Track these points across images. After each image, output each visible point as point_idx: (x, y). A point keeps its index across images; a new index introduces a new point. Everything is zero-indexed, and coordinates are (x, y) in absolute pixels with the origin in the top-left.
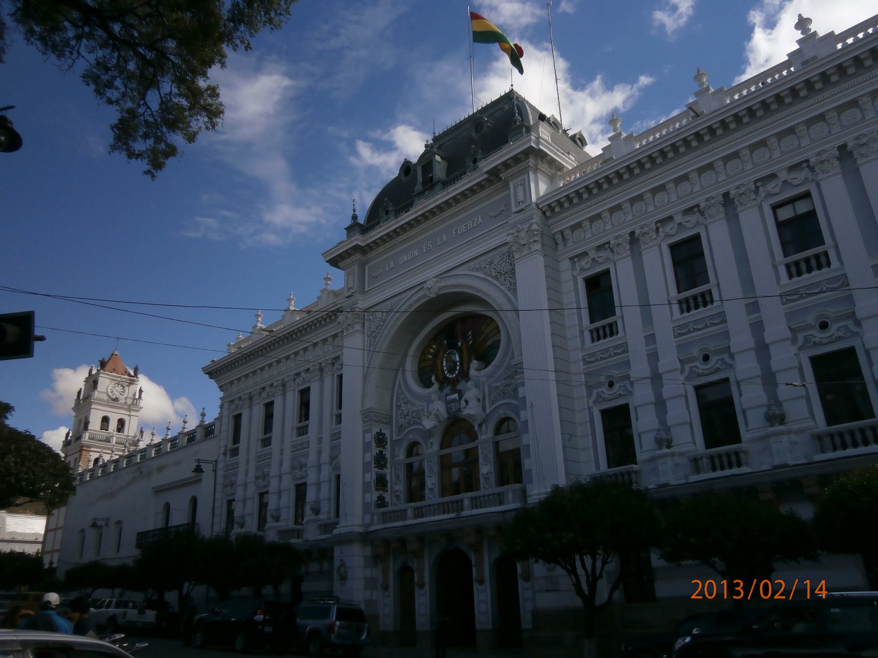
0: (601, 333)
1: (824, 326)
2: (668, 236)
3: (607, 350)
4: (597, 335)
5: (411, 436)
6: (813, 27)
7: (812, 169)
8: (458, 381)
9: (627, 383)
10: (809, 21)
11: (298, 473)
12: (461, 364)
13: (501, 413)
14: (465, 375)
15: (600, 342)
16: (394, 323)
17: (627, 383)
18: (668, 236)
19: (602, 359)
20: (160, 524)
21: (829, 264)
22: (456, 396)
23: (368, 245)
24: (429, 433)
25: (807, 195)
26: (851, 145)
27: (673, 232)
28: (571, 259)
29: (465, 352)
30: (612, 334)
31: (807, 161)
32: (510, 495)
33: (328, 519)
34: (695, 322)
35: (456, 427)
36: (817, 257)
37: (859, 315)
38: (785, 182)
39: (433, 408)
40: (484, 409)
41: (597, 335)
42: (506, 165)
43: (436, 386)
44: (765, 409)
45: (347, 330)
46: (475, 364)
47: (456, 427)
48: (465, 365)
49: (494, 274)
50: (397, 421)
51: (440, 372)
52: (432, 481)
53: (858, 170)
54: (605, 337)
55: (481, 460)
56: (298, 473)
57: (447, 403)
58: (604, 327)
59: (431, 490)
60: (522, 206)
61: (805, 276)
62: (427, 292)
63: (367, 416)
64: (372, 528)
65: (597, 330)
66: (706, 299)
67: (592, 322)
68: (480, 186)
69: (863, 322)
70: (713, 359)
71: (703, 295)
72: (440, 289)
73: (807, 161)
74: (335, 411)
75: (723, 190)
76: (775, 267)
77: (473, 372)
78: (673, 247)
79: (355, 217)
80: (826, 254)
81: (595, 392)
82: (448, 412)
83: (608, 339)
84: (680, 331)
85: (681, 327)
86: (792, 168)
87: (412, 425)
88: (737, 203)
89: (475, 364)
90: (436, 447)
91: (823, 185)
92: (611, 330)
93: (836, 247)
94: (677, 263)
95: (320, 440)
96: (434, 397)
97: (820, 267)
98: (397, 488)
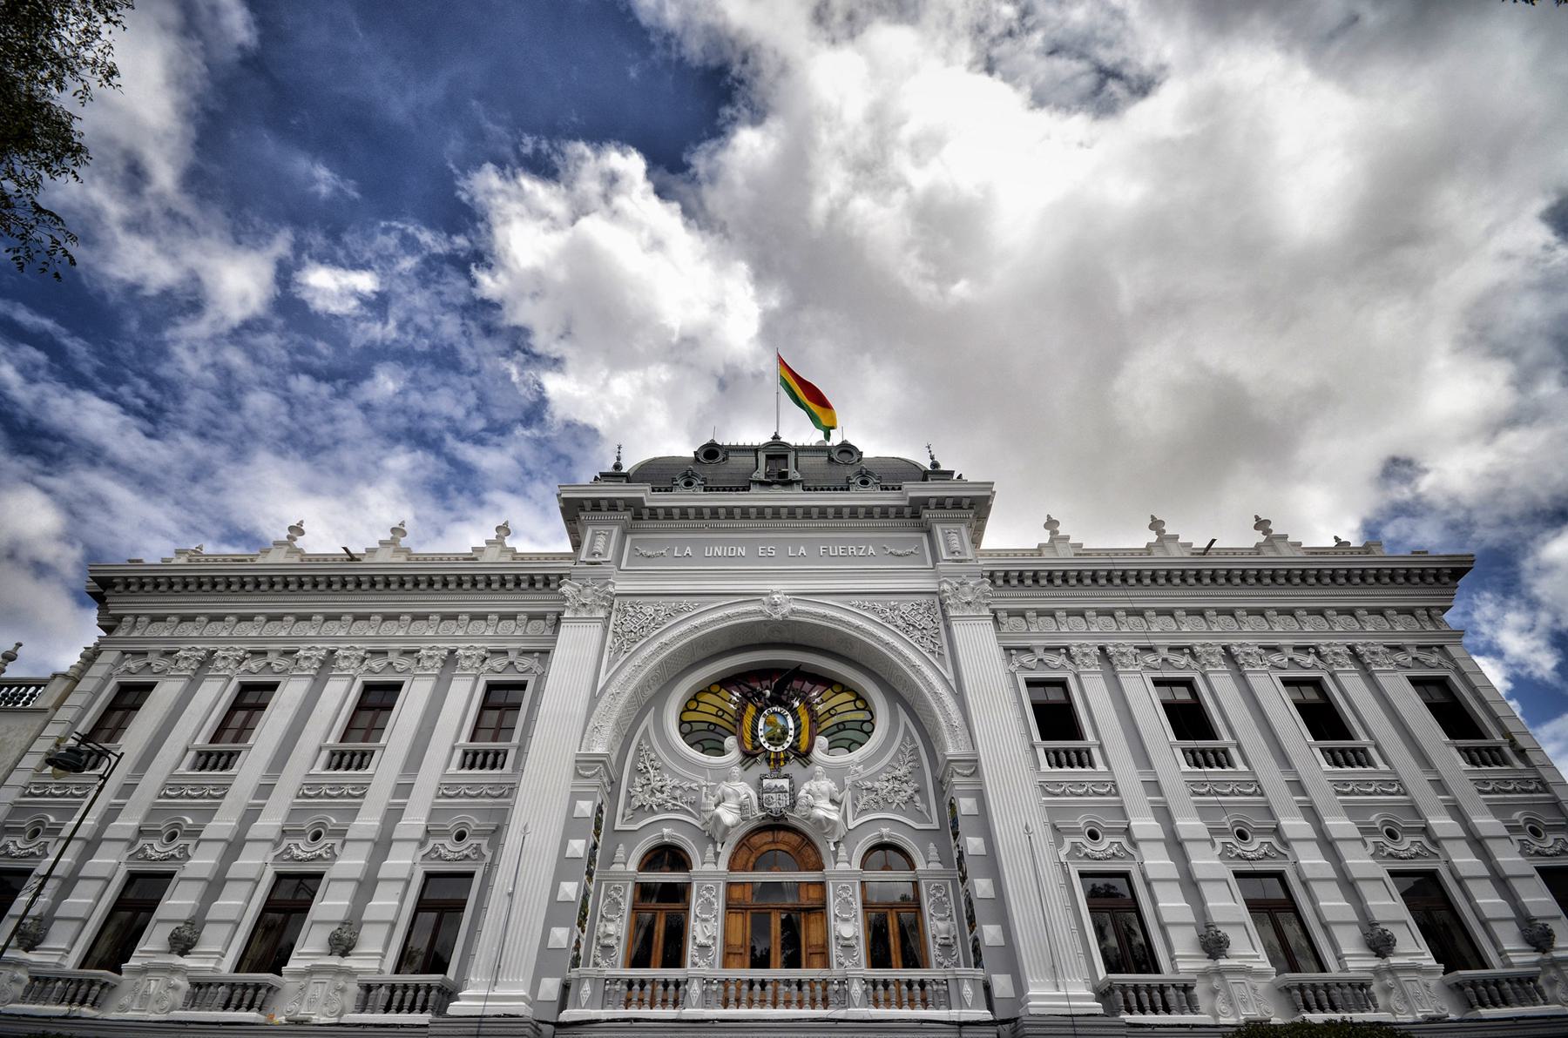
0: (480, 758)
1: (1093, 835)
2: (492, 670)
3: (339, 786)
4: (472, 760)
5: (885, 830)
6: (1169, 530)
7: (1193, 655)
8: (787, 759)
9: (338, 842)
10: (302, 533)
11: (303, 848)
12: (797, 736)
13: (668, 833)
14: (804, 756)
15: (473, 771)
16: (677, 633)
17: (338, 842)
18: (492, 670)
19: (1072, 794)
20: (1335, 885)
21: (1092, 764)
22: (785, 783)
23: (653, 509)
24: (712, 834)
25: (1062, 684)
26: (1110, 649)
27: (499, 668)
28: (124, 653)
29: (805, 719)
30: (493, 766)
31: (1067, 649)
32: (967, 990)
33: (380, 972)
34: (472, 786)
35: (779, 836)
36: (1078, 752)
37: (1137, 834)
38: (512, 663)
39: (732, 793)
40: (845, 817)
41: (472, 760)
42: (941, 504)
43: (734, 755)
44: (335, 927)
45: (576, 610)
46: (822, 741)
47: (779, 836)
48: (805, 737)
49: (900, 622)
50: (630, 796)
51: (748, 736)
52: (706, 927)
53: (1116, 677)
54: (482, 766)
56: (303, 848)
57: (760, 789)
58: (486, 754)
59: (703, 948)
60: (597, 559)
61: (476, 771)
62: (766, 609)
63: (585, 764)
64: (568, 1015)
65: (476, 754)
66: (494, 760)
68: (885, 512)
69: (1141, 845)
70: (469, 841)
71: (497, 754)
72: (793, 612)
73: (1067, 649)
74: (464, 740)
75: (451, 646)
76: (453, 748)
77: (818, 754)
78: (491, 687)
79: (617, 466)
80: (1088, 751)
81: (1068, 841)
82: (761, 807)
83: (485, 771)
84: (447, 789)
85: (450, 786)
86: (1048, 649)
87: (667, 810)
88: (1115, 661)
89: (822, 741)
90: (632, 867)
91: (1084, 678)
92: (360, 760)
93: (1101, 747)
94: (360, 707)
95: (403, 790)
96: (737, 770)
98: (611, 928)
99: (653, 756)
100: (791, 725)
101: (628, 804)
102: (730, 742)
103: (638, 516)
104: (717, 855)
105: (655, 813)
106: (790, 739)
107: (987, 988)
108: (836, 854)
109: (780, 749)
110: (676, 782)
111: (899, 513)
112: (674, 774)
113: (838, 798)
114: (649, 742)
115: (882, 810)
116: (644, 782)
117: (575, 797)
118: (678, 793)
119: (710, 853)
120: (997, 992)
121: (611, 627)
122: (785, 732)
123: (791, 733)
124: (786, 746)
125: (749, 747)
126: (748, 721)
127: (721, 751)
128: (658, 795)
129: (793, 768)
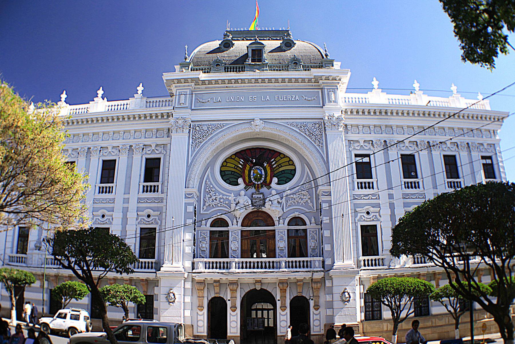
8: (262, 187)
12: (266, 177)
14: (268, 185)
32: (317, 264)
35: (258, 216)
43: (242, 185)
47: (258, 216)
50: (205, 202)
51: (247, 178)
52: (235, 244)
55: (277, 238)
66: (155, 190)
67: (145, 181)
77: (273, 185)
89: (275, 180)
96: (243, 193)
97: (369, 188)
99: (211, 186)
100: (263, 173)
101: (204, 205)
102: (240, 180)
103: (197, 84)
104: (237, 222)
105: (214, 208)
106: (263, 179)
107: (323, 262)
108: (279, 221)
109: (259, 183)
110: (221, 196)
111: (310, 80)
112: (220, 193)
113: (280, 202)
114: (210, 181)
115: (296, 206)
116: (209, 196)
117: (186, 204)
118: (222, 200)
119: (235, 221)
120: (326, 263)
121: (191, 135)
122: (261, 175)
123: (264, 176)
124: (262, 181)
125: (247, 182)
126: (247, 172)
127: (238, 184)
128: (215, 201)
129: (264, 190)
